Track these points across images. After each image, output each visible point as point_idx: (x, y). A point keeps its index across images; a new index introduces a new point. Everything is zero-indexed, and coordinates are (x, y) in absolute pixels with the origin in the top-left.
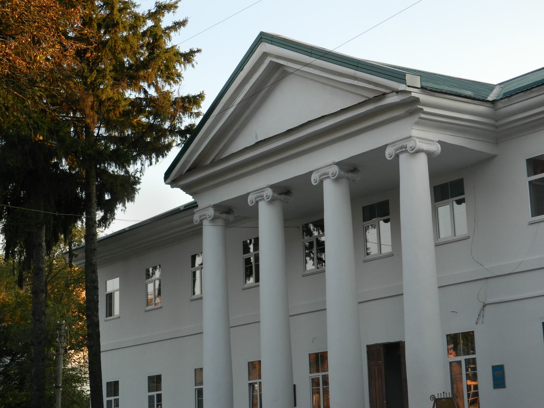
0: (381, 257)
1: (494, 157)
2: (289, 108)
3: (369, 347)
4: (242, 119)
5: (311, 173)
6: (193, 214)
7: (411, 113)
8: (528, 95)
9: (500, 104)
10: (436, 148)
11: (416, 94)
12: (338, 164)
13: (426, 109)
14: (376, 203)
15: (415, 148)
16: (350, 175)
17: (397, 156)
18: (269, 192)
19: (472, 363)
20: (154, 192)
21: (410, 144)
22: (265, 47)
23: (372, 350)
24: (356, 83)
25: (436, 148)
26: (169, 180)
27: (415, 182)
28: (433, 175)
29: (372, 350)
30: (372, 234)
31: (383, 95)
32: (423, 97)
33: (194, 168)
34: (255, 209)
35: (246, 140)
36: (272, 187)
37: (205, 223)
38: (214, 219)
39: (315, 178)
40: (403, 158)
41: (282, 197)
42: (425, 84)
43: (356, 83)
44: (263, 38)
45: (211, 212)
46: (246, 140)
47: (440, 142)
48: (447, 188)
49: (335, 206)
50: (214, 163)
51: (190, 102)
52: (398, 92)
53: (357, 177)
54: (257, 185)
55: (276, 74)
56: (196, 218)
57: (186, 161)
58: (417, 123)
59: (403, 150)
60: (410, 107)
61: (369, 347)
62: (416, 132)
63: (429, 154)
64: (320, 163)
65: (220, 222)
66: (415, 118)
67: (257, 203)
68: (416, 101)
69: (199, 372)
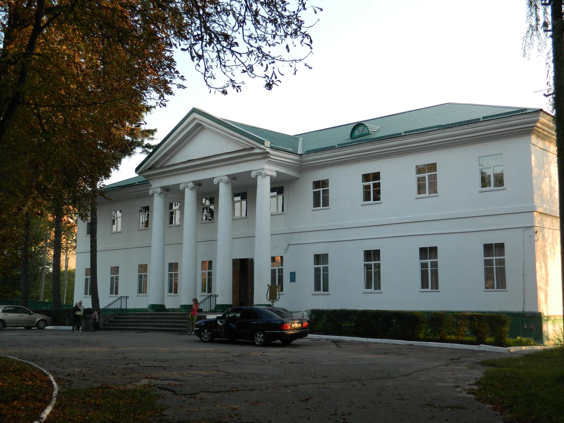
0: (241, 218)
1: (298, 178)
2: (204, 146)
3: (233, 260)
4: (179, 147)
5: (214, 178)
6: (149, 189)
7: (265, 158)
8: (317, 154)
9: (304, 156)
10: (274, 174)
11: (268, 150)
12: (228, 176)
13: (272, 157)
14: (244, 190)
15: (266, 171)
16: (232, 181)
17: (257, 176)
18: (191, 185)
19: (281, 271)
20: (126, 170)
21: (263, 172)
22: (195, 115)
23: (235, 262)
24: (240, 140)
25: (274, 174)
26: (138, 172)
27: (264, 187)
28: (272, 183)
29: (235, 262)
30: (237, 205)
31: (253, 149)
32: (271, 152)
33: (151, 168)
34: (183, 193)
35: (180, 158)
36: (193, 182)
37: (155, 195)
38: (160, 194)
39: (215, 181)
40: (259, 178)
41: (197, 187)
42: (272, 145)
43: (240, 140)
44: (194, 110)
45: (159, 190)
46: (180, 158)
47: (276, 171)
48: (278, 188)
49: (224, 192)
50: (161, 167)
51: (152, 132)
52: (260, 148)
53: (235, 182)
54: (185, 180)
55: (199, 128)
56: (151, 192)
57: (148, 164)
58: (267, 162)
59: (260, 174)
60: (265, 155)
61: (233, 260)
62: (266, 166)
63: (271, 177)
64: (219, 174)
65: (163, 195)
66: (267, 160)
67: (184, 188)
68: (268, 153)
69: (143, 268)
